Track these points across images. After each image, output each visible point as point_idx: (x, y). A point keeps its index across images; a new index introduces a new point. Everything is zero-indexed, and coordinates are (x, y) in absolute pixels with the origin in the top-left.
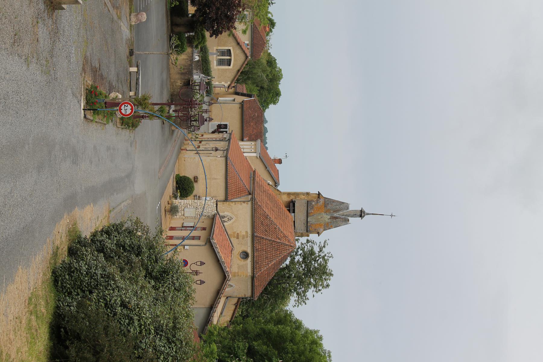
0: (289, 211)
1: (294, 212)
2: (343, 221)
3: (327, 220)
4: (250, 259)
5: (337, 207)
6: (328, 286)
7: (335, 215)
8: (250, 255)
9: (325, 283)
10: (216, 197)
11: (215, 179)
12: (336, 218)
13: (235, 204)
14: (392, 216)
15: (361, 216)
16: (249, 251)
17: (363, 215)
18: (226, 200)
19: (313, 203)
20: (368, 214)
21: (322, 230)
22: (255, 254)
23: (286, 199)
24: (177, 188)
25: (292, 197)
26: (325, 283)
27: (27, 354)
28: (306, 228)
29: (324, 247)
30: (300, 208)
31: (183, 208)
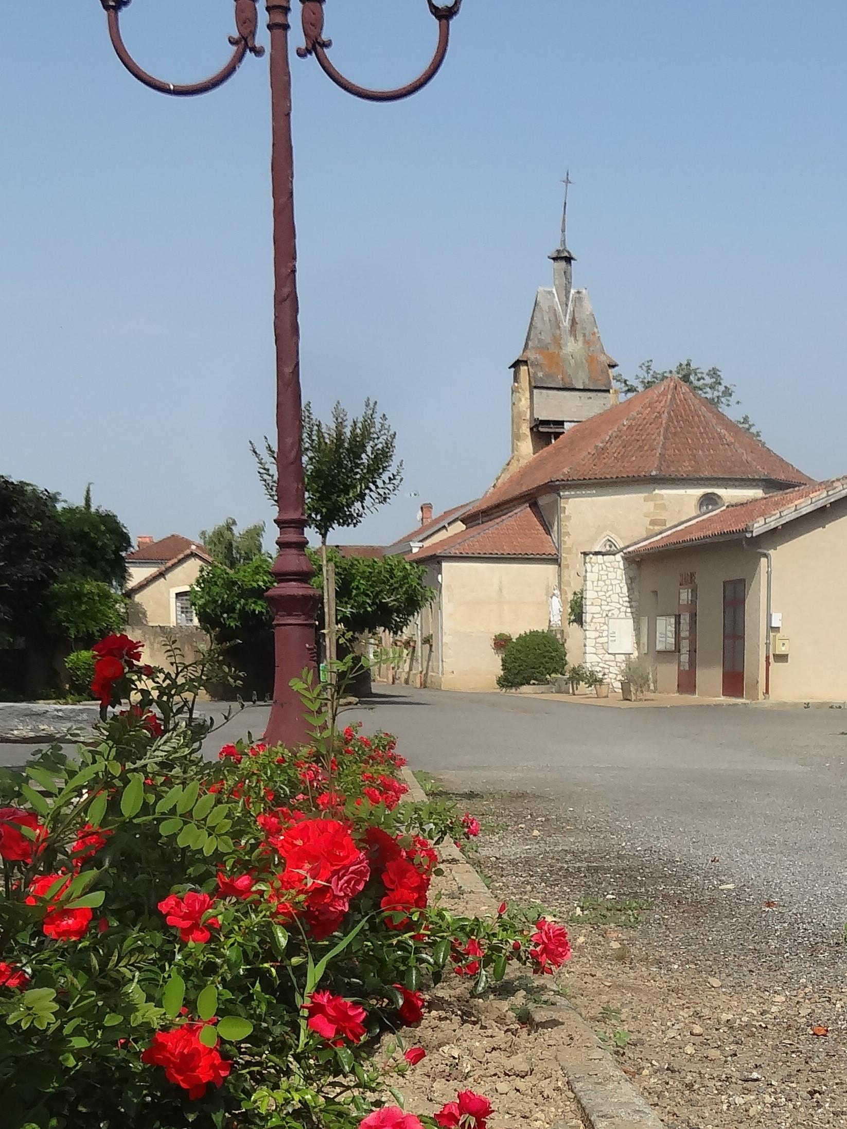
0: (557, 435)
1: (561, 423)
2: (581, 306)
3: (580, 344)
4: (720, 491)
5: (546, 318)
6: (714, 373)
7: (566, 324)
8: (710, 490)
9: (709, 380)
10: (548, 587)
11: (501, 590)
12: (573, 322)
13: (568, 534)
14: (567, 181)
15: (568, 260)
16: (699, 492)
17: (566, 254)
18: (554, 560)
19: (540, 374)
20: (564, 242)
21: (602, 358)
22: (707, 474)
23: (526, 446)
24: (542, 681)
25: (525, 429)
26: (709, 380)
27: (302, 897)
28: (600, 394)
29: (625, 382)
30: (552, 406)
31: (607, 657)
